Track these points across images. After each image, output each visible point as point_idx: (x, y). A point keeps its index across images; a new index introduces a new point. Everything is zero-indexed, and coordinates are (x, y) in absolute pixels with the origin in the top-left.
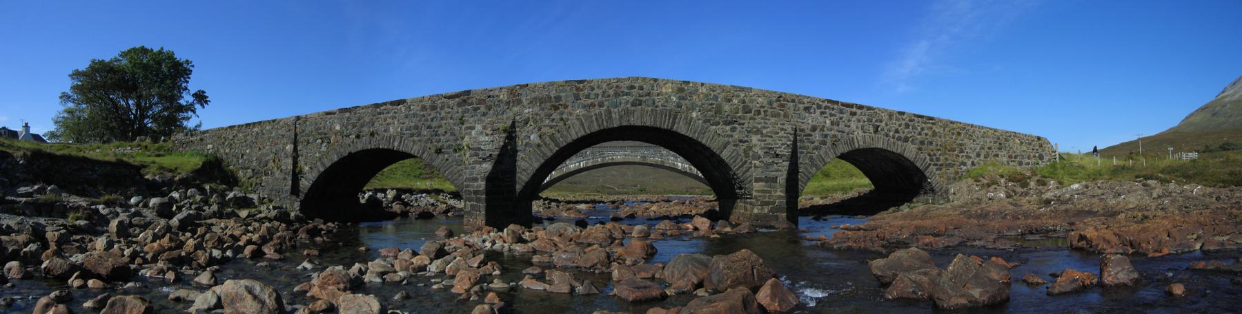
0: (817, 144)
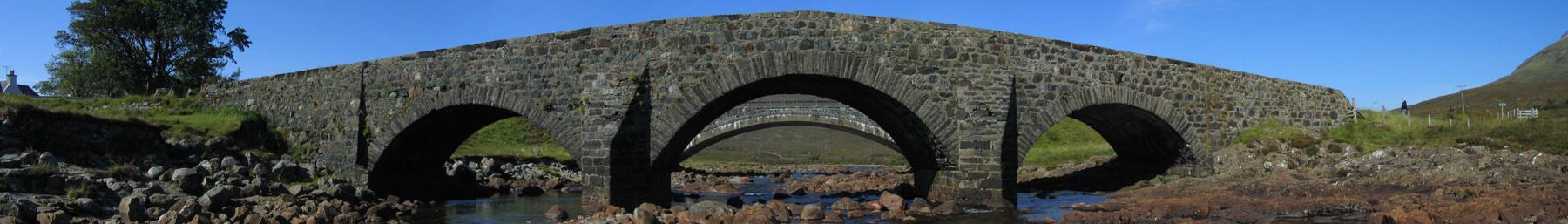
0: (1042, 98)
